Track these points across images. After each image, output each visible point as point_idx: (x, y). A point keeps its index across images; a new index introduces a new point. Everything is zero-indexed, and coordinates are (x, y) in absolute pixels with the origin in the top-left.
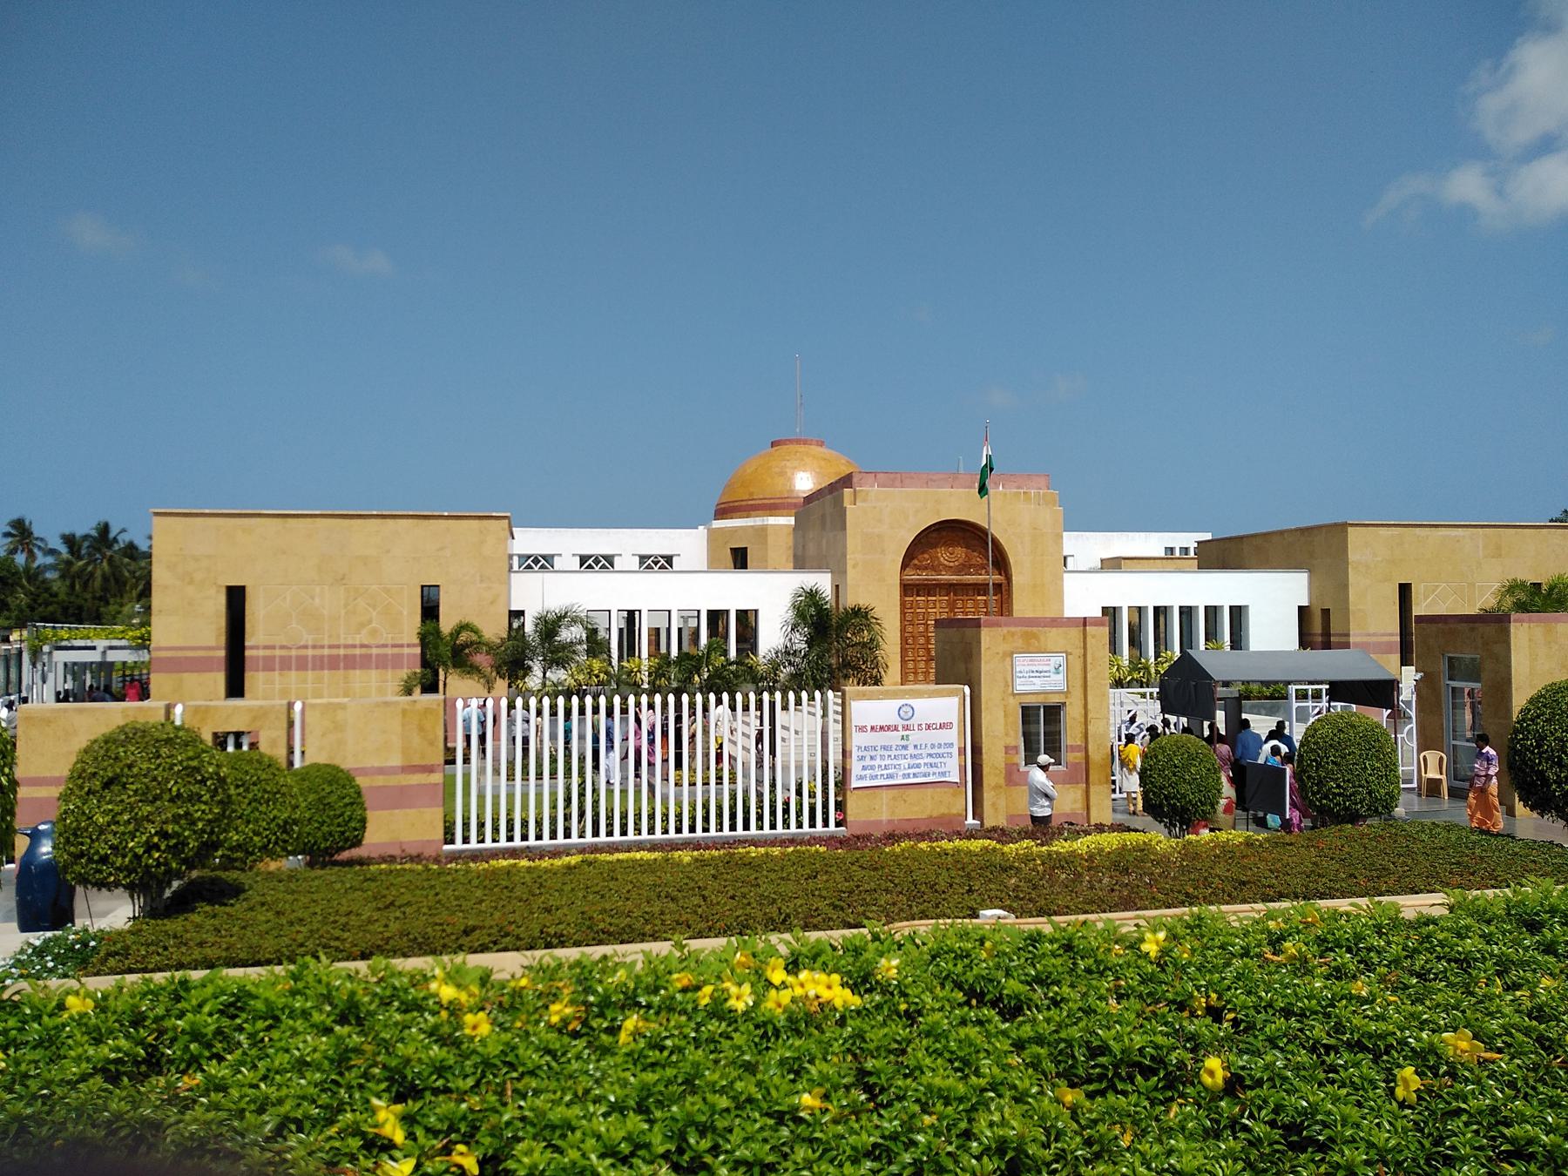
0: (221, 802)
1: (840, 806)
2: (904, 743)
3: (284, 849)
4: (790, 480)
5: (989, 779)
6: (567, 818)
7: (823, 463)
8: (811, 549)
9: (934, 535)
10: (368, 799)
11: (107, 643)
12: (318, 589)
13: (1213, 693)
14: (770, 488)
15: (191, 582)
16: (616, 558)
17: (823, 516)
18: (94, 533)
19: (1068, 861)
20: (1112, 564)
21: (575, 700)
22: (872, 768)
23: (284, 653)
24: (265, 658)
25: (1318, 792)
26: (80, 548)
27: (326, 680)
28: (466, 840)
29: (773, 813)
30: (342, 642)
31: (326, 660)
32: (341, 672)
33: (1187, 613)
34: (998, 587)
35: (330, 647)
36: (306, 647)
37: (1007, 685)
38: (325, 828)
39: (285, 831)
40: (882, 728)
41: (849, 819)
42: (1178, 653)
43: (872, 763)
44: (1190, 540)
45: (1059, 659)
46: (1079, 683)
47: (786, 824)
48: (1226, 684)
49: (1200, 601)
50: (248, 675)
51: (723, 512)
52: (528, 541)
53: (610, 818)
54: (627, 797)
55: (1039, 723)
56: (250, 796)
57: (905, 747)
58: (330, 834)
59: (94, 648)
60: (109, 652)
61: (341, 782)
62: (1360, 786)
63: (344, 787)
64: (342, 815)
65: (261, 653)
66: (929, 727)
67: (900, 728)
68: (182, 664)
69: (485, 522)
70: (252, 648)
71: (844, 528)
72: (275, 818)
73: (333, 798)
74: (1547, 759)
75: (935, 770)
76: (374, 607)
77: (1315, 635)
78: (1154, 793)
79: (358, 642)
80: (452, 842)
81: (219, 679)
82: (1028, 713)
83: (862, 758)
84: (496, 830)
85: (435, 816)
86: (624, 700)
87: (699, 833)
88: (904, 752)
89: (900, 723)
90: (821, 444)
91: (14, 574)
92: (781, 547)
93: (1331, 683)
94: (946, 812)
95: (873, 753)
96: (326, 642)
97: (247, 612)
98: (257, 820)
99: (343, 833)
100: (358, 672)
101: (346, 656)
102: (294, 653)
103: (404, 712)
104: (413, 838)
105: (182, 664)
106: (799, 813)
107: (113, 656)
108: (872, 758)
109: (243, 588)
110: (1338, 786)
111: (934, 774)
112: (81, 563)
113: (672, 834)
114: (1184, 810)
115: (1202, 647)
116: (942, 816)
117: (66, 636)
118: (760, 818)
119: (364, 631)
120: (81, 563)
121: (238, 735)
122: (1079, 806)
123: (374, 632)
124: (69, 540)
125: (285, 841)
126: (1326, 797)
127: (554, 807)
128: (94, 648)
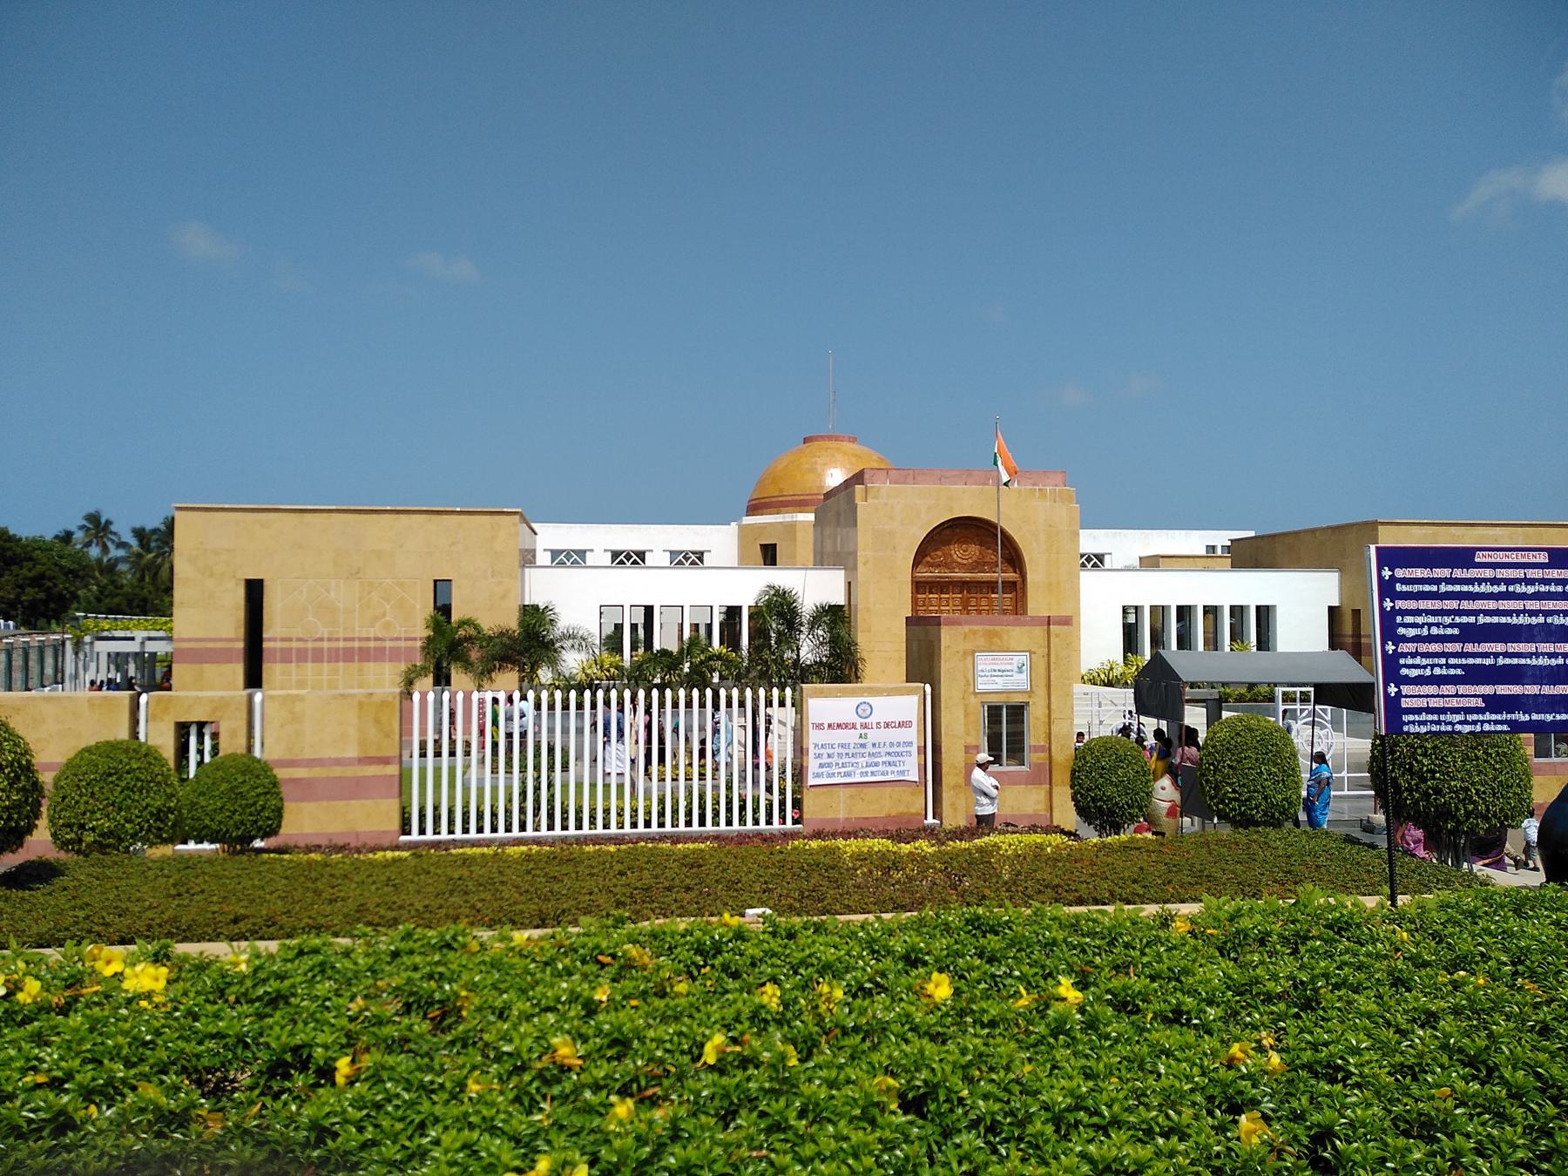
0: (24, 789)
1: (797, 804)
2: (862, 741)
3: (160, 837)
4: (821, 476)
5: (947, 780)
6: (523, 811)
7: (853, 459)
8: (828, 548)
9: (947, 532)
10: (285, 790)
11: (146, 634)
12: (333, 583)
13: (1181, 694)
14: (804, 484)
15: (211, 575)
16: (588, 554)
17: (838, 514)
18: (163, 528)
19: (371, 863)
20: (1151, 563)
21: (587, 693)
22: (829, 765)
23: (301, 645)
24: (299, 650)
25: (1215, 797)
26: (149, 541)
27: (341, 672)
28: (422, 831)
29: (729, 810)
30: (357, 635)
31: (341, 652)
32: (356, 665)
33: (1212, 611)
34: (1010, 586)
35: (345, 639)
36: (321, 639)
37: (968, 684)
38: (237, 817)
39: (158, 819)
40: (839, 726)
41: (805, 816)
42: (1148, 656)
43: (830, 760)
44: (1222, 538)
45: (1023, 658)
46: (1043, 682)
47: (742, 821)
48: (1193, 685)
49: (1225, 601)
50: (265, 666)
51: (754, 509)
52: (551, 536)
53: (565, 812)
54: (568, 791)
55: (1001, 722)
56: (123, 784)
57: (863, 746)
58: (242, 823)
59: (132, 639)
60: (148, 643)
61: (256, 773)
62: (1255, 791)
63: (258, 777)
64: (254, 804)
65: (279, 645)
66: (887, 725)
67: (858, 726)
68: (203, 655)
69: (497, 518)
70: (270, 640)
71: (856, 525)
72: (148, 805)
73: (244, 789)
74: (1401, 765)
75: (893, 768)
76: (388, 600)
77: (1345, 636)
78: (1082, 795)
79: (372, 636)
80: (409, 833)
81: (238, 670)
82: (994, 712)
83: (819, 756)
84: (451, 822)
85: (392, 807)
86: (742, 693)
87: (654, 828)
88: (862, 750)
89: (858, 721)
90: (853, 440)
91: (84, 568)
92: (805, 545)
93: (1317, 686)
94: (905, 810)
95: (830, 751)
96: (341, 635)
97: (265, 605)
98: (129, 808)
99: (255, 822)
100: (372, 664)
101: (360, 649)
102: (310, 645)
103: (361, 704)
104: (367, 829)
105: (203, 655)
106: (756, 810)
107: (151, 647)
108: (829, 756)
109: (261, 582)
110: (1234, 791)
111: (893, 772)
112: (150, 556)
113: (627, 829)
114: (1111, 812)
115: (1227, 649)
116: (900, 816)
117: (107, 627)
118: (716, 814)
119: (378, 625)
120: (150, 556)
121: (201, 725)
122: (1041, 808)
123: (387, 626)
124: (140, 534)
125: (159, 829)
126: (1222, 802)
127: (509, 800)
128: (132, 639)
